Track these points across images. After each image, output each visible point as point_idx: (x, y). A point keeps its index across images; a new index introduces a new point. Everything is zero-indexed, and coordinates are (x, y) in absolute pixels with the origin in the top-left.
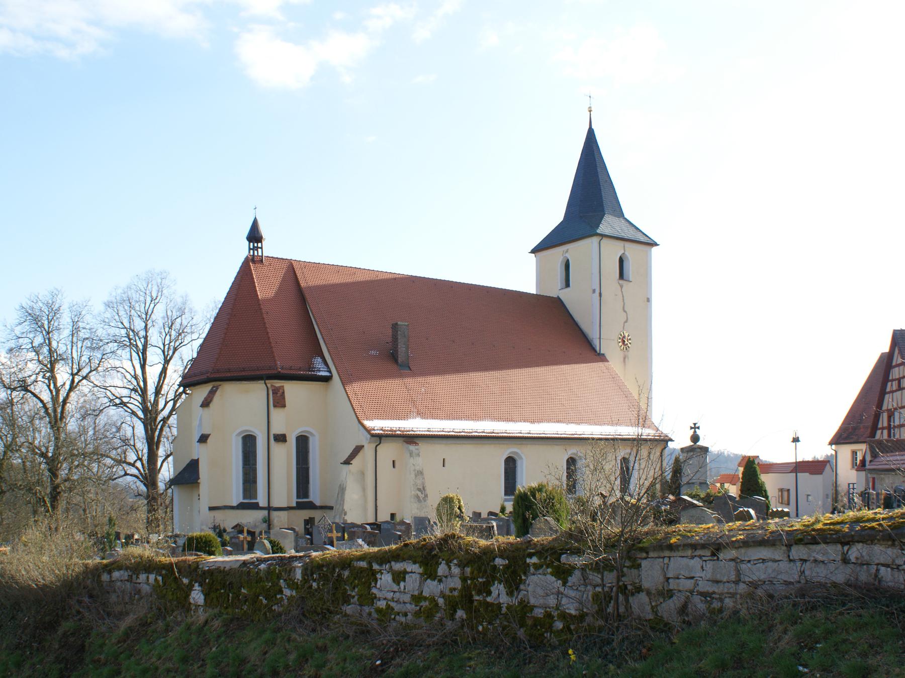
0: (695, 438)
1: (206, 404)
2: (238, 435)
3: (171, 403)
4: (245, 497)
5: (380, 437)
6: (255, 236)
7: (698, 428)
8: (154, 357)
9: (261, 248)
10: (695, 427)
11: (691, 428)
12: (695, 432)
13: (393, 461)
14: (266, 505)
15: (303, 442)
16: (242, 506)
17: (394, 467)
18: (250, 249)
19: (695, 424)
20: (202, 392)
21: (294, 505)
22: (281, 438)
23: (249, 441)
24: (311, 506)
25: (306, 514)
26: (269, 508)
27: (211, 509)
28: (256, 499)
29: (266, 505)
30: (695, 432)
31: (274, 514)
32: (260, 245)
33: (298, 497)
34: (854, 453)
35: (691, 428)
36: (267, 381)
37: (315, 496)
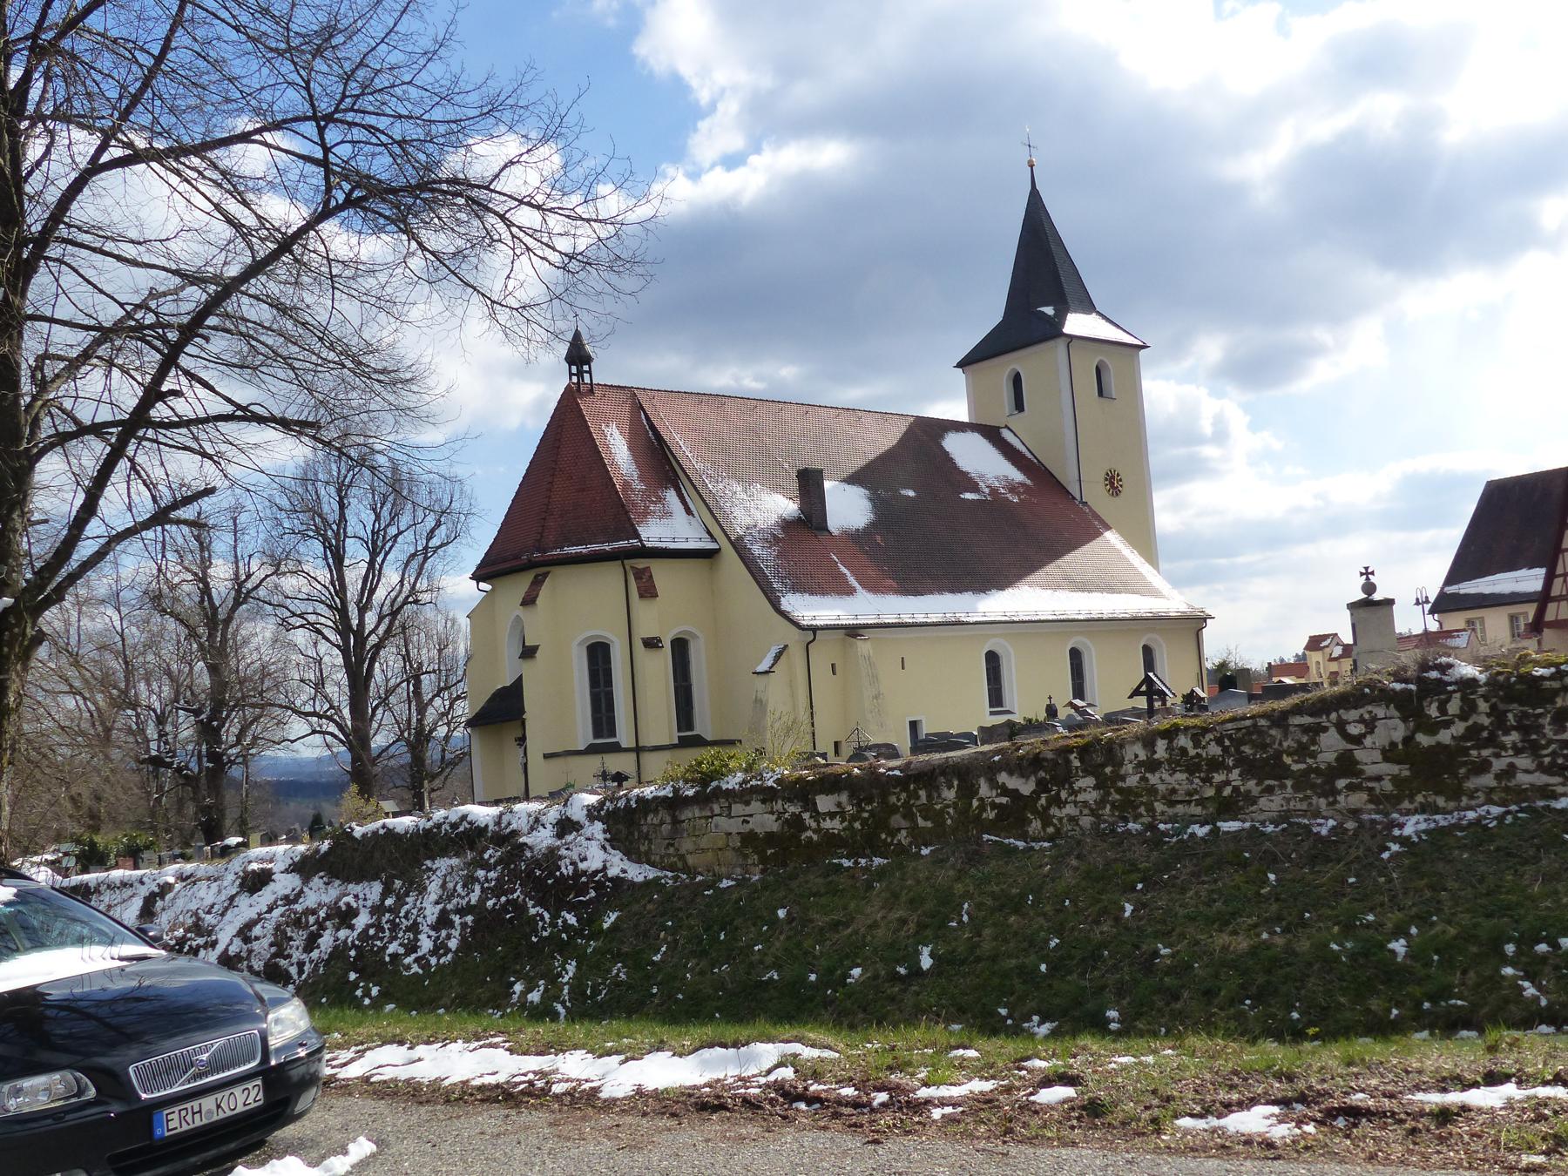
0: (1369, 588)
1: (529, 601)
2: (580, 644)
3: (387, 621)
4: (597, 735)
5: (814, 630)
6: (578, 357)
7: (1372, 573)
8: (356, 554)
9: (590, 372)
10: (1367, 573)
11: (1362, 574)
12: (1368, 579)
13: (833, 665)
14: (634, 745)
15: (680, 647)
16: (592, 750)
17: (834, 673)
18: (571, 374)
19: (1367, 568)
20: (522, 584)
21: (676, 742)
22: (652, 644)
23: (598, 654)
24: (699, 742)
25: (690, 756)
26: (638, 750)
27: (546, 756)
28: (613, 734)
29: (634, 745)
30: (1368, 579)
31: (648, 758)
32: (586, 368)
33: (679, 730)
34: (1513, 619)
35: (1362, 574)
36: (626, 562)
37: (704, 725)
